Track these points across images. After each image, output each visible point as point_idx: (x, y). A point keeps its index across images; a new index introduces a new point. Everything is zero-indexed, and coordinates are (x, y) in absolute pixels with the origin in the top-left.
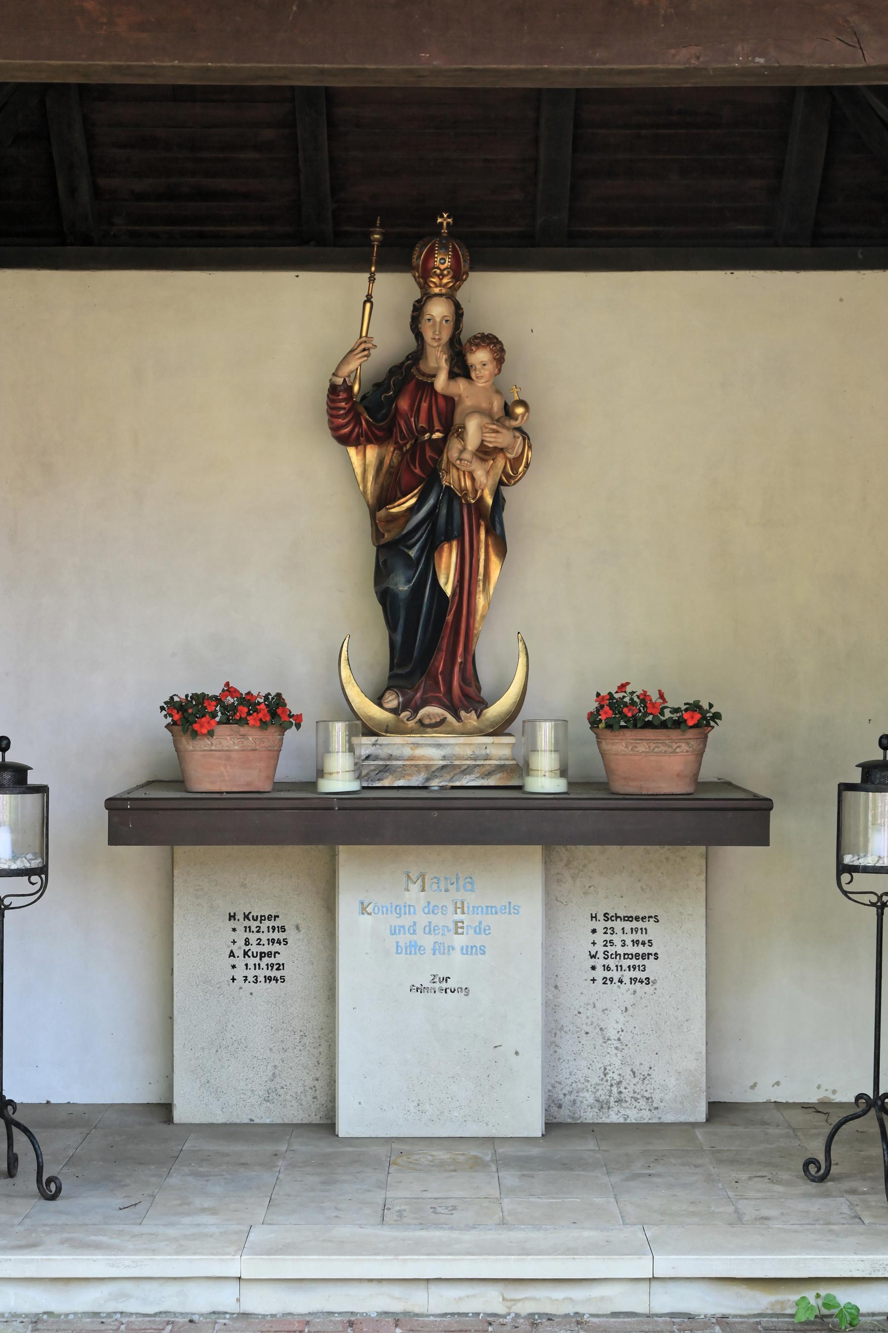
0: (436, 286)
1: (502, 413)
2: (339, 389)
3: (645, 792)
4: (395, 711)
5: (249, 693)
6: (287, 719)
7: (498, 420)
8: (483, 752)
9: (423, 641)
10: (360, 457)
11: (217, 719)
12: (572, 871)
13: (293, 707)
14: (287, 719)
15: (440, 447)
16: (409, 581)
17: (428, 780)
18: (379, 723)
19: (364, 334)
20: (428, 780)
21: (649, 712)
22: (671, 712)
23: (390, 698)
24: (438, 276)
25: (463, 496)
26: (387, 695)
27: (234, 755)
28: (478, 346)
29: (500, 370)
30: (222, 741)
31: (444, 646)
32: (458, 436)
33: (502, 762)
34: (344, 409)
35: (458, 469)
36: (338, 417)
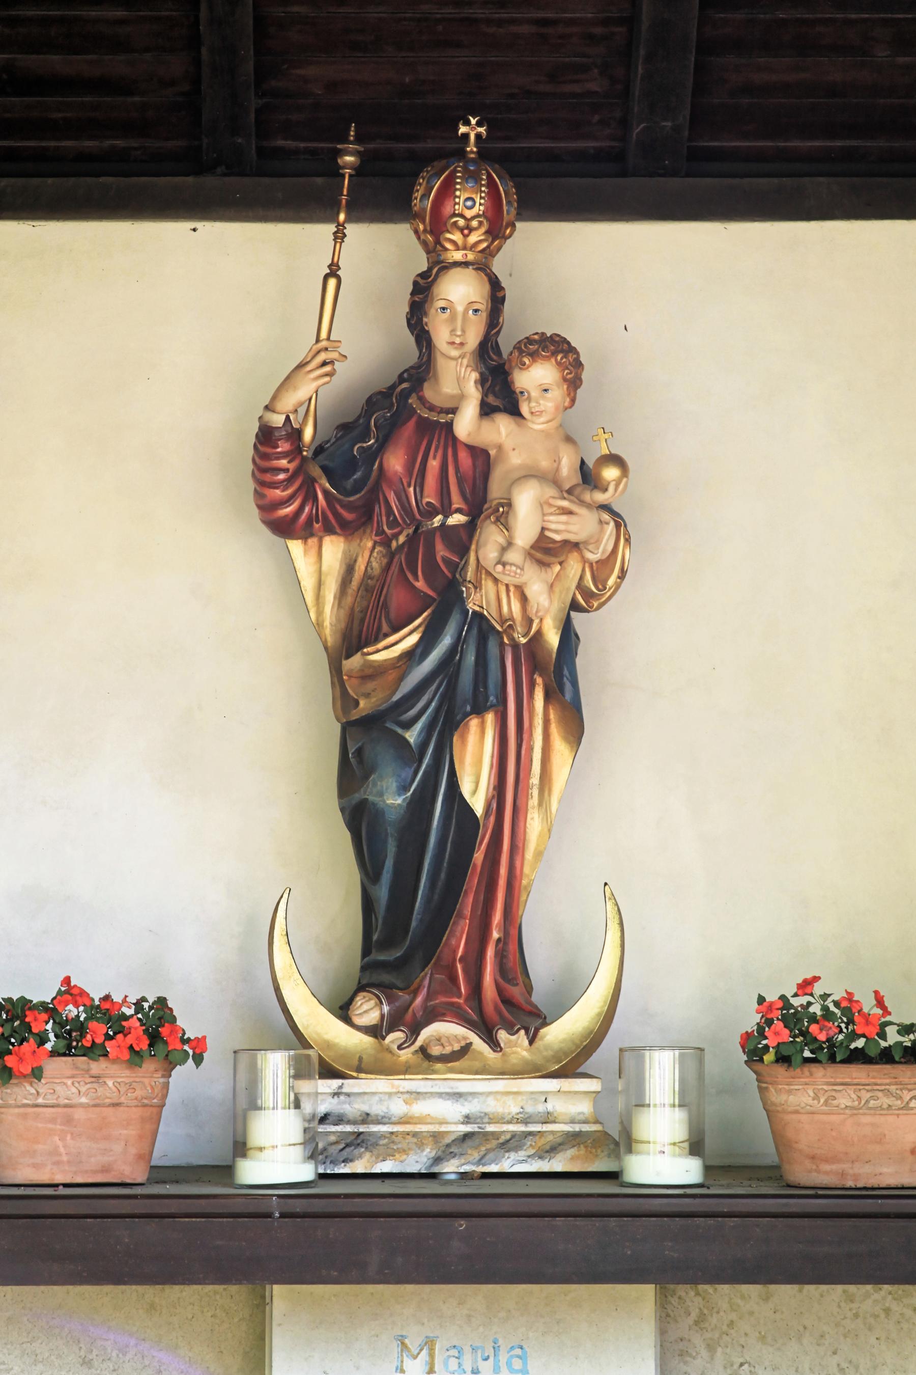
0: (458, 248)
1: (577, 479)
2: (277, 434)
3: (850, 1184)
4: (375, 1031)
5: (107, 998)
6: (178, 1046)
7: (570, 491)
8: (541, 1108)
9: (428, 900)
10: (312, 558)
11: (49, 1046)
12: (708, 1335)
13: (189, 1023)
14: (178, 1046)
15: (462, 541)
16: (404, 788)
17: (437, 1160)
18: (345, 1055)
19: (324, 335)
20: (437, 1160)
21: (859, 1032)
22: (899, 1032)
23: (365, 1007)
24: (461, 230)
25: (505, 631)
26: (359, 1000)
27: (79, 1115)
28: (534, 356)
29: (573, 401)
30: (58, 1088)
31: (468, 911)
32: (498, 520)
33: (577, 1128)
34: (286, 470)
35: (496, 581)
36: (274, 485)
